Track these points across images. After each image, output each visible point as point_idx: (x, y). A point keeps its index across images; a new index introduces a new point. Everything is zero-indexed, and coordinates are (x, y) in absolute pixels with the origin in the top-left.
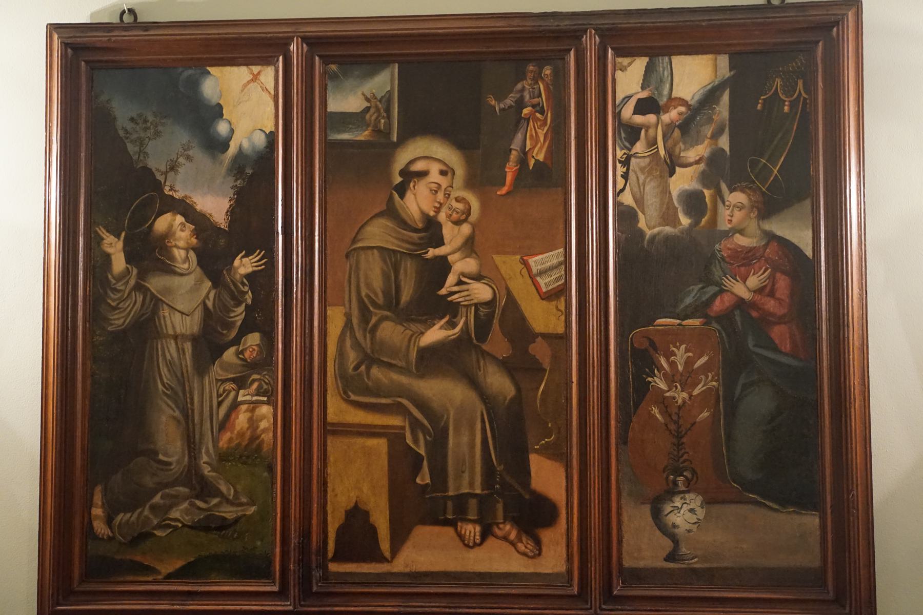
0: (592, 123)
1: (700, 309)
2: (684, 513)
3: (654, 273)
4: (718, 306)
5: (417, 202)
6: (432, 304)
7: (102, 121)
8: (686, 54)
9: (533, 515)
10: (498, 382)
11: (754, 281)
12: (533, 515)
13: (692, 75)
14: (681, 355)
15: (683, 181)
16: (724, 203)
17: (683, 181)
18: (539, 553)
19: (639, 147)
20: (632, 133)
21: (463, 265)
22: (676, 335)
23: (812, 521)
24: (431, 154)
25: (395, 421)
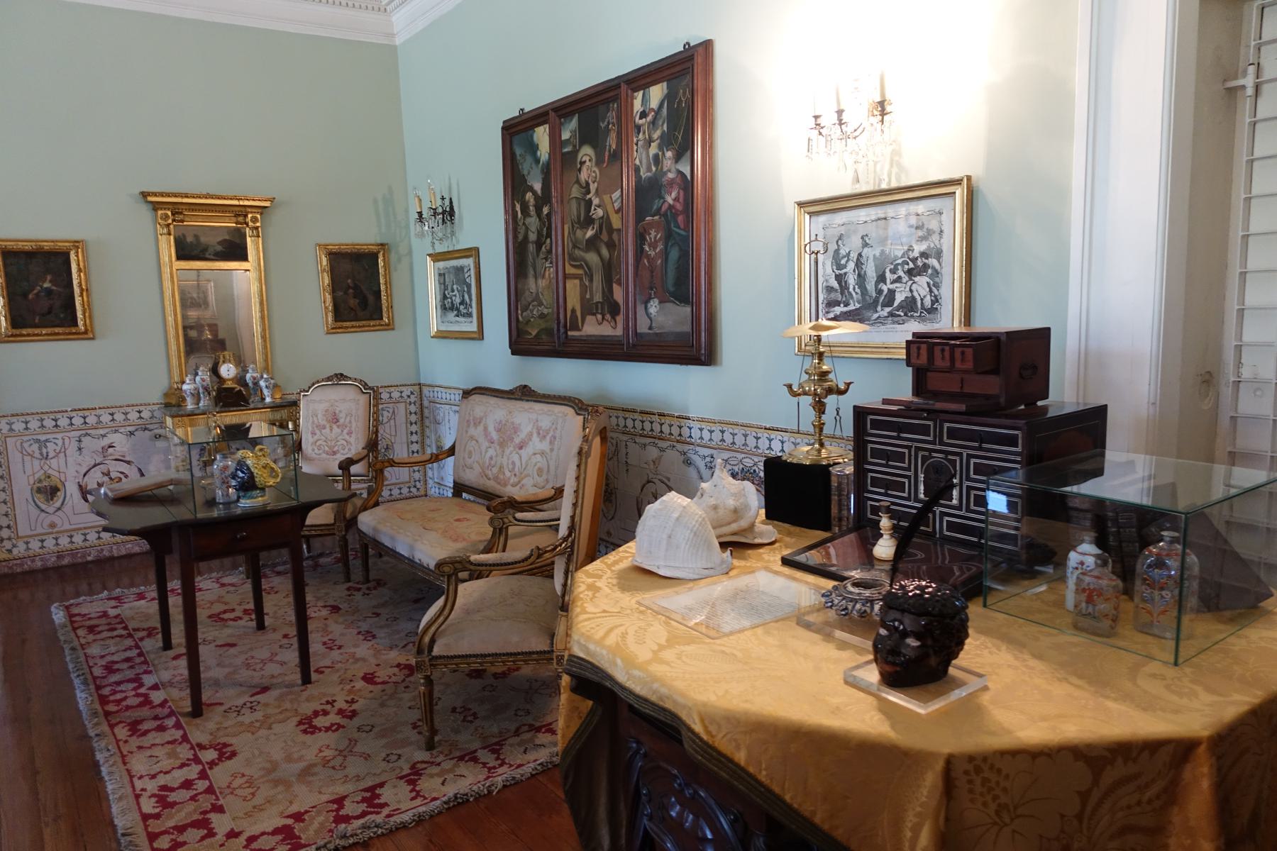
0: (625, 126)
1: (658, 212)
2: (654, 307)
3: (648, 191)
4: (664, 209)
5: (584, 176)
6: (589, 221)
7: (513, 155)
8: (681, 364)
9: (614, 309)
10: (605, 252)
11: (674, 195)
12: (614, 309)
13: (657, 93)
14: (653, 233)
15: (653, 150)
16: (1009, 666)
17: (653, 150)
18: (615, 328)
19: (641, 136)
20: (638, 128)
21: (596, 201)
22: (651, 225)
23: (688, 309)
24: (587, 152)
25: (581, 272)
